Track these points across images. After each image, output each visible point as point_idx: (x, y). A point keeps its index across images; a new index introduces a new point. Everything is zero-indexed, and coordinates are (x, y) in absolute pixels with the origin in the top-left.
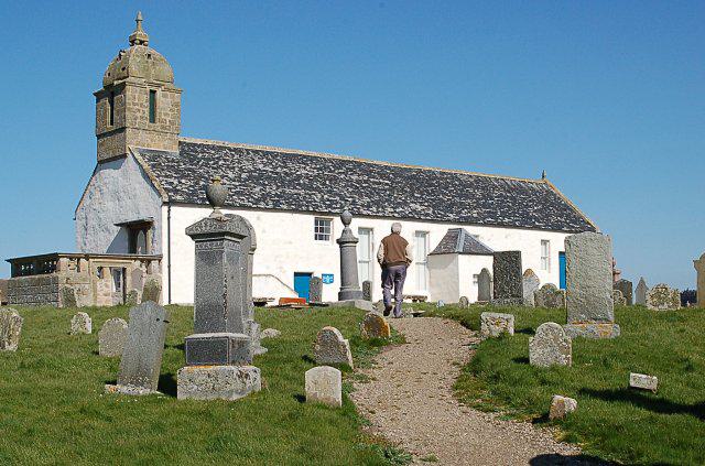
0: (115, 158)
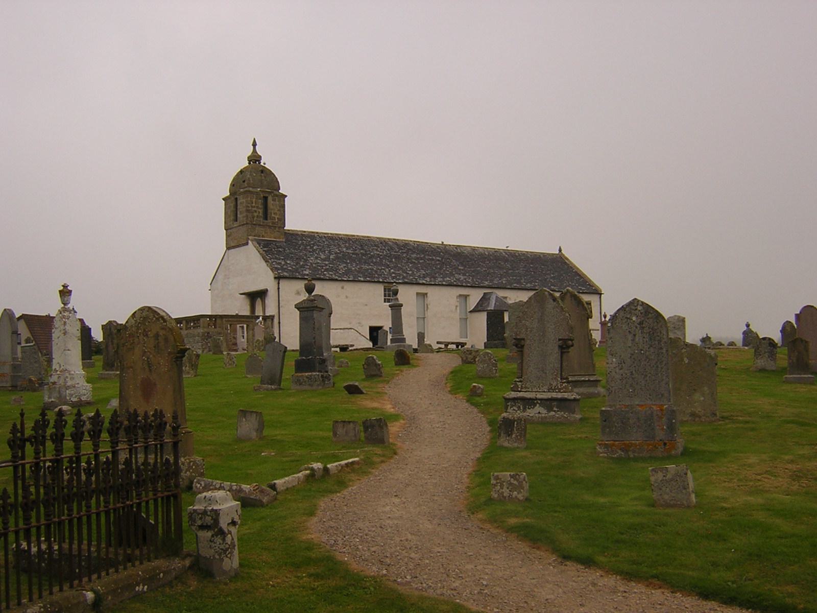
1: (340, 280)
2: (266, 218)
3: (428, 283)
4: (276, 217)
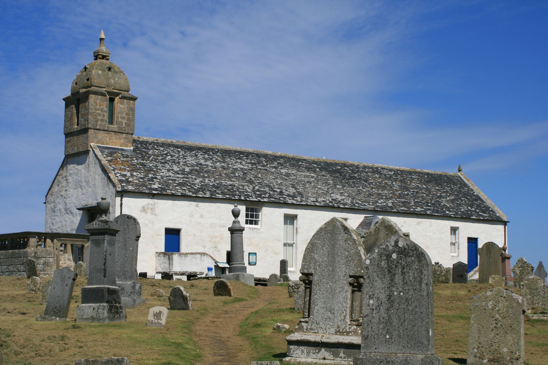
0: (78, 154)
1: (194, 197)
2: (111, 122)
3: (298, 203)
4: (124, 121)
